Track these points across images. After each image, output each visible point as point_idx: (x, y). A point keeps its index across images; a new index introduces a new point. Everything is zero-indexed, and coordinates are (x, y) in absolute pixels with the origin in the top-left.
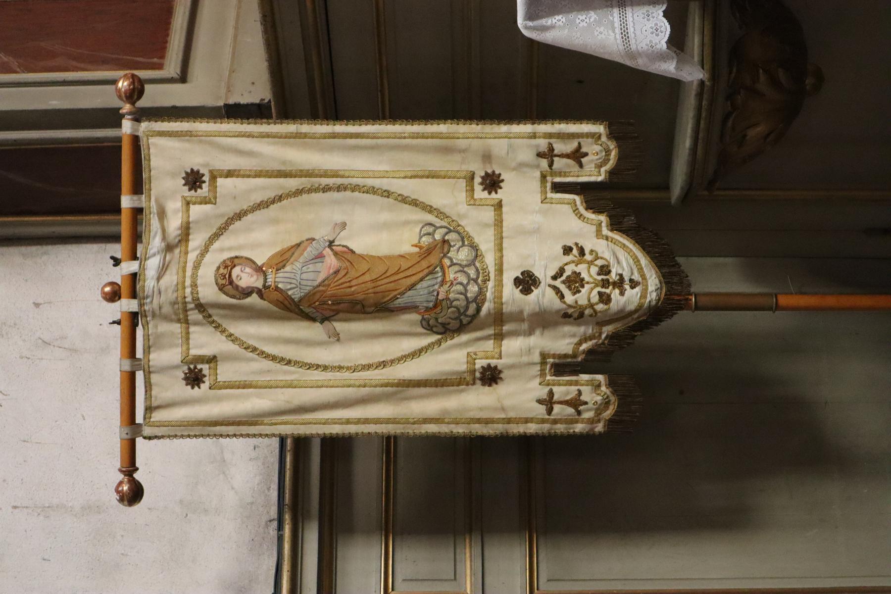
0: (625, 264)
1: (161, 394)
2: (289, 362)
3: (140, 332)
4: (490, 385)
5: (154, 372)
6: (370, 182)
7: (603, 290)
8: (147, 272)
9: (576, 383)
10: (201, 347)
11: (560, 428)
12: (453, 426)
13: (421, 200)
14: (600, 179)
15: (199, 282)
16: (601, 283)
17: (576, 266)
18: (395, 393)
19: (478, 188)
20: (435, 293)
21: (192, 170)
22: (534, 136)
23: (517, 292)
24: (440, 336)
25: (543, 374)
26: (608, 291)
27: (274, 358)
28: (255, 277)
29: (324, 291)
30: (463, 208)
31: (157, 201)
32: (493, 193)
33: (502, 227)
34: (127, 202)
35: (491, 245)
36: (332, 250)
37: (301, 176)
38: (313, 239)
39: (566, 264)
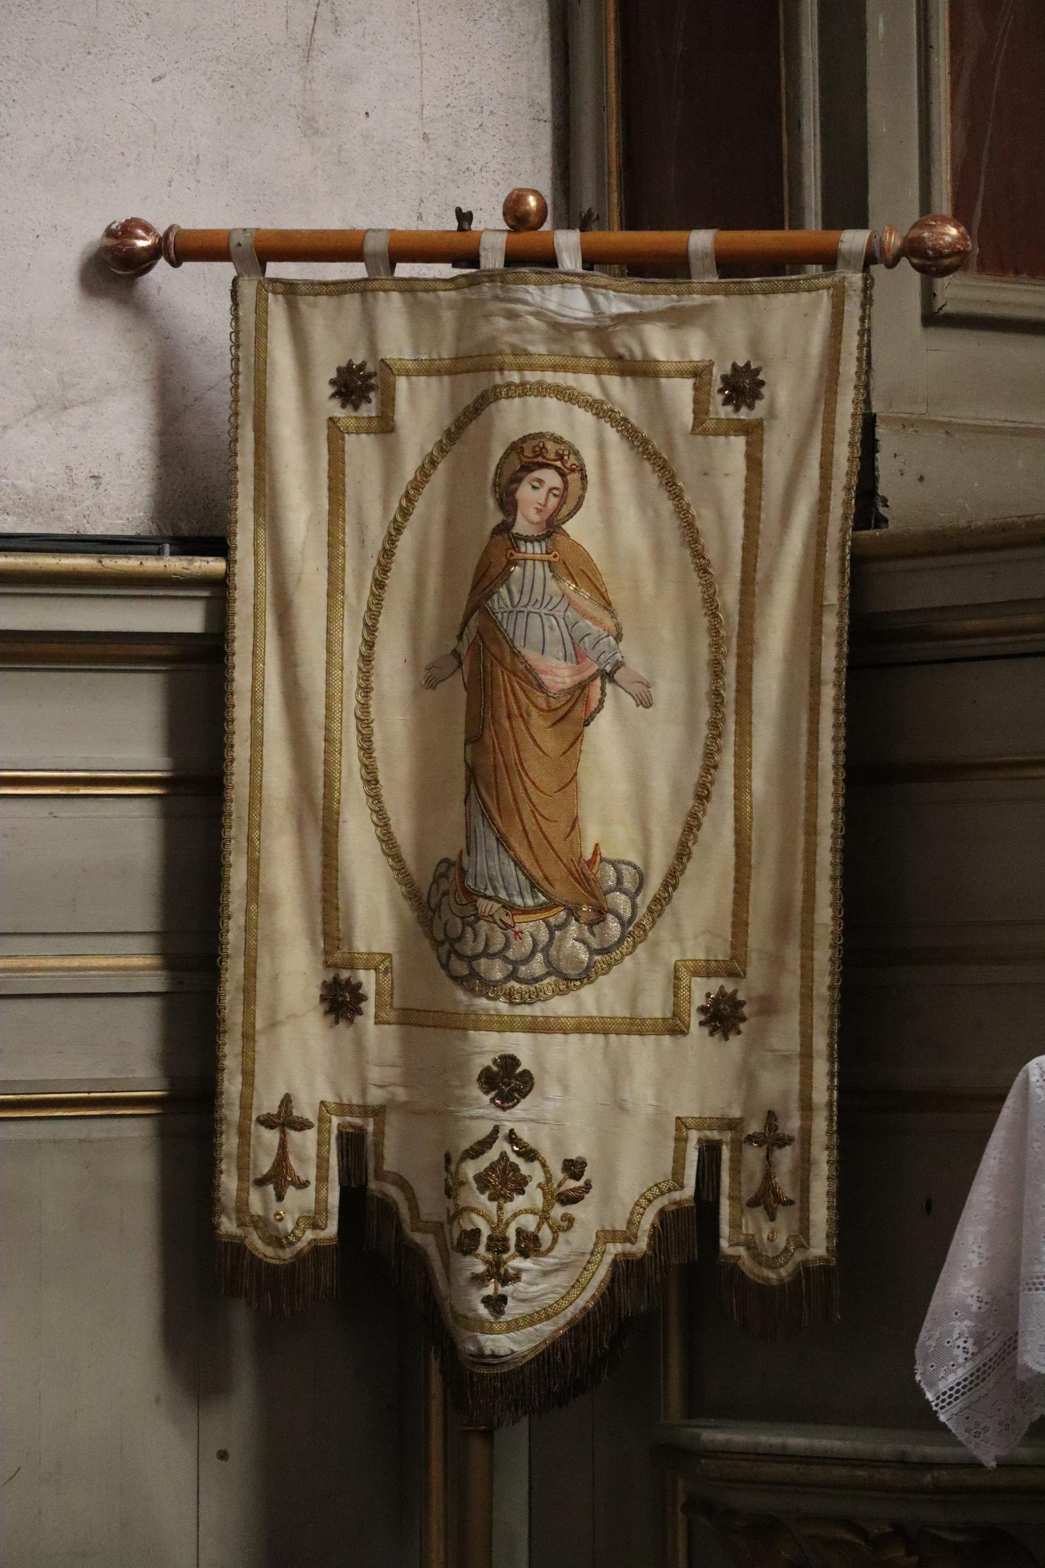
0: (543, 1286)
1: (318, 316)
2: (379, 585)
3: (444, 270)
4: (323, 999)
5: (364, 301)
6: (728, 760)
7: (484, 1240)
8: (556, 289)
9: (322, 1178)
10: (413, 402)
11: (229, 1143)
12: (242, 921)
13: (690, 866)
14: (724, 1243)
15: (531, 400)
16: (497, 1233)
17: (539, 1186)
18: (311, 802)
19: (714, 985)
20: (490, 892)
21: (762, 383)
22: (807, 1107)
23: (487, 1061)
24: (425, 898)
25: (343, 1109)
26: (482, 1250)
27: (387, 553)
28: (536, 518)
29: (501, 663)
30: (671, 954)
31: (704, 307)
32: (703, 1018)
33: (629, 1033)
34: (701, 240)
35: (590, 1008)
36: (592, 678)
37: (741, 614)
38: (618, 638)
39: (544, 1165)
